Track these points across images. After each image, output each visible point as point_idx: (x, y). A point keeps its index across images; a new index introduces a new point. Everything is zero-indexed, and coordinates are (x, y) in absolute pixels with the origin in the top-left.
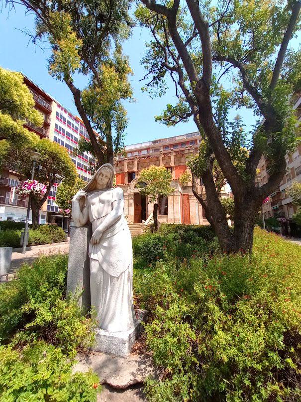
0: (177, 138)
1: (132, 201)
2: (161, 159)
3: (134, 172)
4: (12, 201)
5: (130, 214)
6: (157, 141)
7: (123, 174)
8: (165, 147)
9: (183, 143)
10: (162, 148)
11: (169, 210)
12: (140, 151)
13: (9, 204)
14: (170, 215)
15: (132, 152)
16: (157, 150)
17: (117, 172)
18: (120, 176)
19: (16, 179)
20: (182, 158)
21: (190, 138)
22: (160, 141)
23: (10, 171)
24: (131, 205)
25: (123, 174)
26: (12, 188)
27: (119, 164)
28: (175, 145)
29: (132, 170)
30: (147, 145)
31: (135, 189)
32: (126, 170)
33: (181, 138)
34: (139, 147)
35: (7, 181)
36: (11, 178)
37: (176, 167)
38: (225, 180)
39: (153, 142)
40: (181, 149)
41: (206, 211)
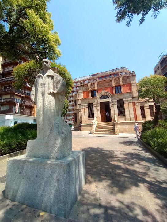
0: (106, 73)
1: (99, 108)
2: (113, 80)
3: (95, 90)
4: (18, 112)
5: (98, 116)
6: (94, 75)
7: (88, 92)
8: (99, 78)
9: (110, 75)
10: (97, 79)
11: (126, 113)
12: (84, 81)
13: (15, 113)
14: (127, 115)
15: (76, 83)
16: (94, 80)
17: (84, 91)
18: (86, 93)
19: (20, 99)
20: (128, 79)
21: (114, 72)
22: (96, 74)
23: (15, 93)
24: (98, 110)
25: (88, 92)
26: (17, 103)
27: (84, 86)
28: (106, 76)
29: (94, 89)
30: (89, 77)
31: (100, 100)
32: (90, 89)
33: (109, 72)
34: (84, 78)
35: (14, 99)
36: (16, 98)
37: (124, 85)
38: (160, 111)
39: (92, 75)
40: (104, 80)
41: (160, 199)
